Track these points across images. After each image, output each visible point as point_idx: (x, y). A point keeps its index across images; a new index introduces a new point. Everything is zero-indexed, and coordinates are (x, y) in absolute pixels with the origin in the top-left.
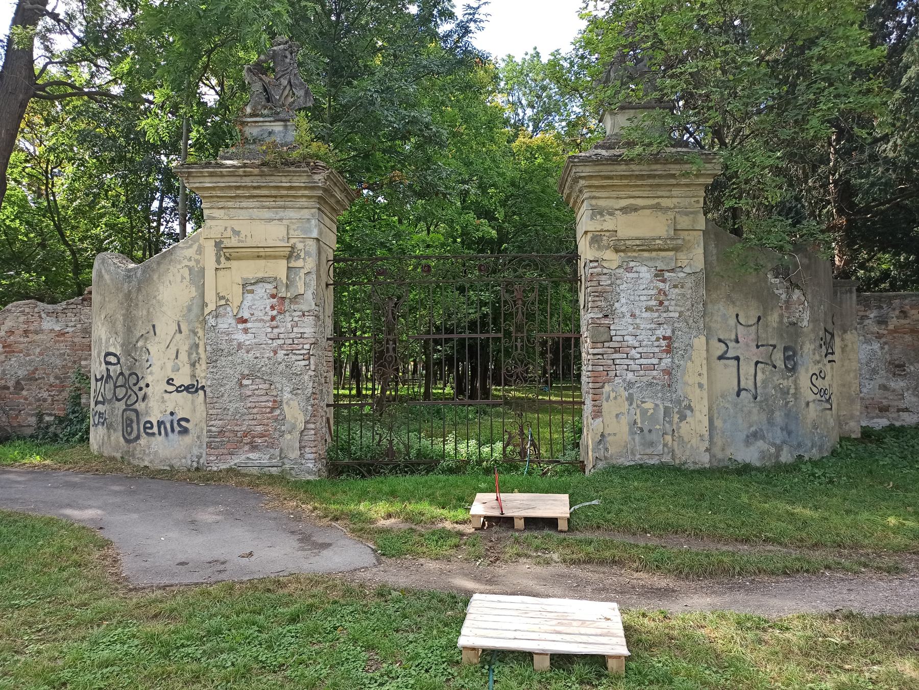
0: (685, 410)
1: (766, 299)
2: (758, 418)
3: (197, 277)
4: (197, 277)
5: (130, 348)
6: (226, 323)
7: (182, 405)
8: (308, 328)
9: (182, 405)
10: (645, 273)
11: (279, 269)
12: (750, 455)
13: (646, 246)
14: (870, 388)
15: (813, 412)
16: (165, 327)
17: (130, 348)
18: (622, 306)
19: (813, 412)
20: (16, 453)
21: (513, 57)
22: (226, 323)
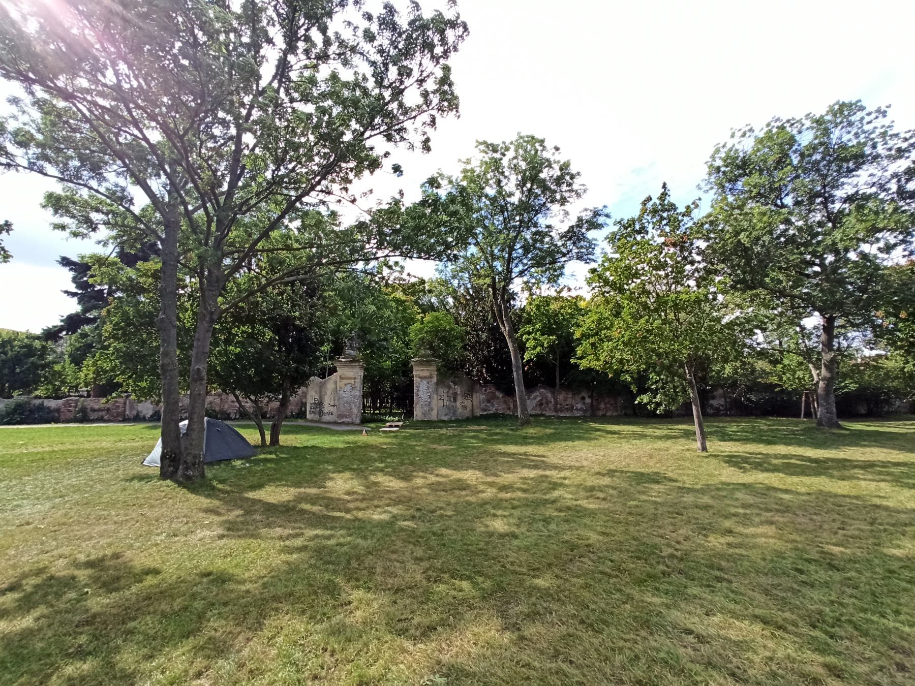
0: (432, 409)
1: (449, 388)
2: (447, 411)
3: (336, 383)
4: (336, 383)
5: (321, 397)
6: (341, 392)
7: (332, 409)
8: (358, 393)
9: (332, 409)
10: (425, 382)
11: (352, 381)
12: (446, 418)
13: (425, 377)
14: (483, 405)
15: (460, 410)
16: (329, 393)
17: (321, 397)
18: (421, 389)
19: (460, 410)
20: (119, 294)
21: (622, 220)
22: (341, 392)
